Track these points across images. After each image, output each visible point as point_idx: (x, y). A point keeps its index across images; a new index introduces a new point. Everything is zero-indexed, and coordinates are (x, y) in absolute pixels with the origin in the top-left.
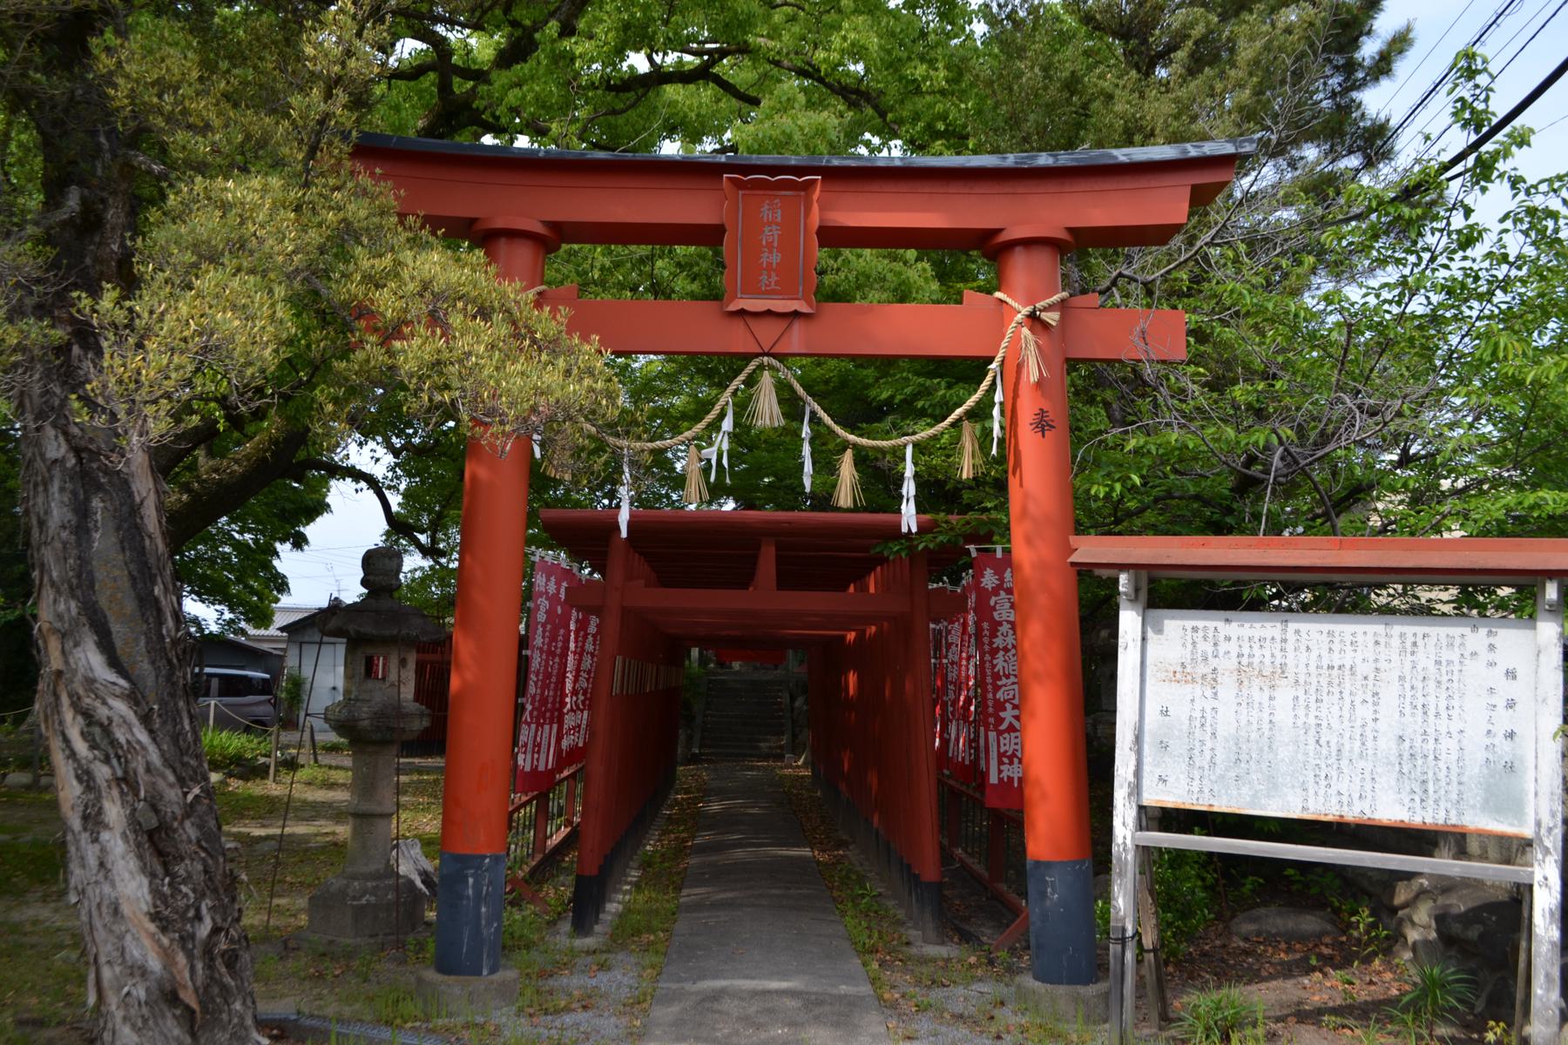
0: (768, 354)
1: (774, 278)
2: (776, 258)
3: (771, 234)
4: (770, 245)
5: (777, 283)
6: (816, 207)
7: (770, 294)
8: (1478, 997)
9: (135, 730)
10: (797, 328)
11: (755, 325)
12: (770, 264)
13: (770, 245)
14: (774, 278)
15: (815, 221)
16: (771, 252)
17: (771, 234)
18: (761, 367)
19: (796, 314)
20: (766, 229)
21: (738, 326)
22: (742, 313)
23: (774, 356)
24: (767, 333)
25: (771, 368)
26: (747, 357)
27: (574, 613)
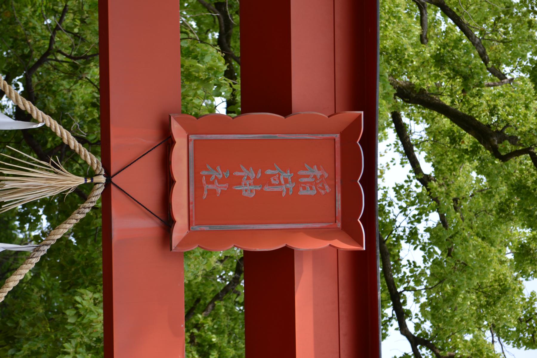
0: (108, 184)
1: (219, 188)
2: (248, 190)
3: (282, 182)
4: (265, 180)
5: (212, 192)
6: (322, 244)
7: (196, 182)
8: (477, 178)
9: (54, 125)
10: (150, 225)
11: (151, 162)
12: (239, 181)
13: (265, 180)
14: (219, 188)
15: (304, 244)
16: (256, 182)
17: (282, 182)
18: (91, 174)
19: (168, 223)
20: (288, 175)
21: (149, 137)
22: (167, 142)
23: (106, 196)
24: (140, 180)
25: (91, 187)
26: (103, 147)
27: (34, 218)
